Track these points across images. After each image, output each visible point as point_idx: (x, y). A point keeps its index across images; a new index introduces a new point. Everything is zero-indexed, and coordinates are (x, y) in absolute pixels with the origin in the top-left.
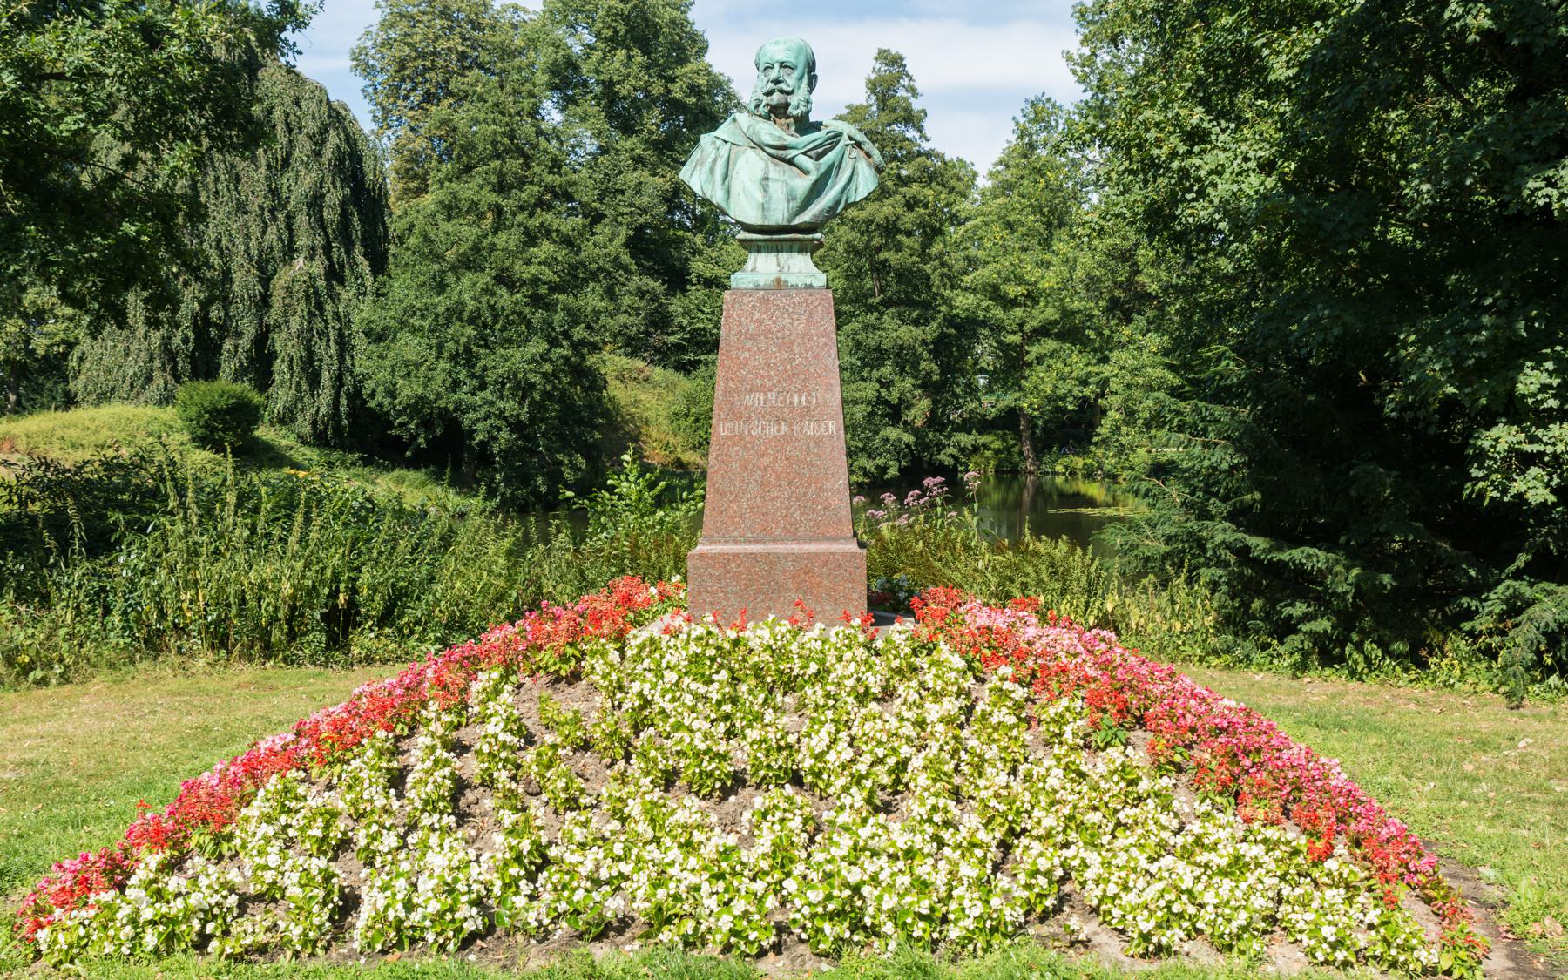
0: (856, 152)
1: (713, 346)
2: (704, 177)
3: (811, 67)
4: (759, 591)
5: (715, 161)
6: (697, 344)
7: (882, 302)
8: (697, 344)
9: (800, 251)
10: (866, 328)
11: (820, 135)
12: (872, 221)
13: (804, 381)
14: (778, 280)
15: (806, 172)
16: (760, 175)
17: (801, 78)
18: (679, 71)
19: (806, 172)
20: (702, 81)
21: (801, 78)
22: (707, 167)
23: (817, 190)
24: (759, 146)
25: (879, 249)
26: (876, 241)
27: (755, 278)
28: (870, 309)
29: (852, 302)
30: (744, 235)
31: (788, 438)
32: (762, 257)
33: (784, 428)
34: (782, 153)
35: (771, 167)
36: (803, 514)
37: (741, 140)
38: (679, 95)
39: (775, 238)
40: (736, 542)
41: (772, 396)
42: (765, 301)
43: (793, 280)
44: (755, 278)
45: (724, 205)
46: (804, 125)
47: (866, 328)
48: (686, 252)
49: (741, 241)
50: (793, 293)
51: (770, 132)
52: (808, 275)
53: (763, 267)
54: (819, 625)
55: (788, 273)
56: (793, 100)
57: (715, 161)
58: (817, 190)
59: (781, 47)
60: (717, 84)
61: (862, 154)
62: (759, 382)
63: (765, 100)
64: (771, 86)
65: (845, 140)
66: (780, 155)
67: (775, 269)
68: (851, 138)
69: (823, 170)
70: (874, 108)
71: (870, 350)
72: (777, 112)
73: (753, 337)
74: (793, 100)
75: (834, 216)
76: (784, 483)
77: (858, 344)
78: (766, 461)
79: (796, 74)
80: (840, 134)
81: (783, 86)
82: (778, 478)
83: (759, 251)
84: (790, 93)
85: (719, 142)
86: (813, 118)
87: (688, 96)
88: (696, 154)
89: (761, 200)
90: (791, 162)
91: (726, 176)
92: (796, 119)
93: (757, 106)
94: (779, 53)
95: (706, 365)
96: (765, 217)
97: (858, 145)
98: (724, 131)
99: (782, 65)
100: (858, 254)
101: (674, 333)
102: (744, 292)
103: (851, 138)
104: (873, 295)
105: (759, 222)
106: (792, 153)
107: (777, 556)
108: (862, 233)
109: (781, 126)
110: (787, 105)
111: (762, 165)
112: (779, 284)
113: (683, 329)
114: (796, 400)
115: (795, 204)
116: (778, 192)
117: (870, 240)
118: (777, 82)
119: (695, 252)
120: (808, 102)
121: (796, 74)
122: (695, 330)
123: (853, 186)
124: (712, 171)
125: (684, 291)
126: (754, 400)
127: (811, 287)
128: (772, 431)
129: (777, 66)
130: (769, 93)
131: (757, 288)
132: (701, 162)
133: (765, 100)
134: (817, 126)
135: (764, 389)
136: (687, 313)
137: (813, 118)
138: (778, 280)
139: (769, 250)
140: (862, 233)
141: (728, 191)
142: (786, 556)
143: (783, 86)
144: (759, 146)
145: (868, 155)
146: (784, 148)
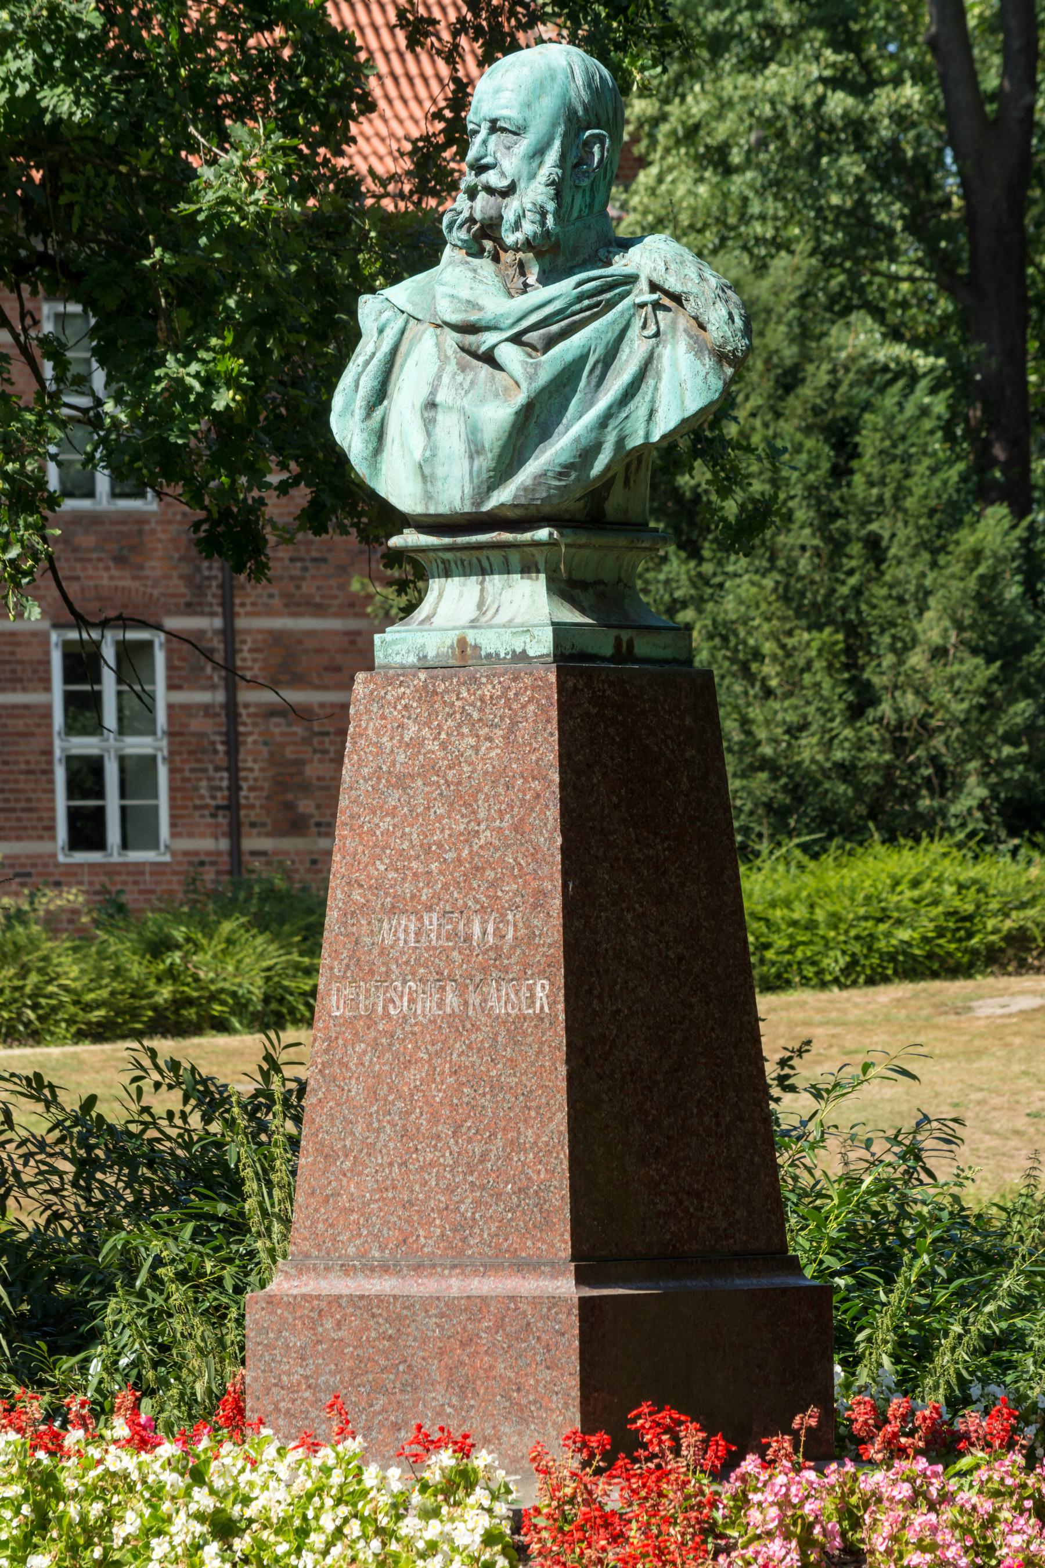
4: (378, 1388)
13: (493, 885)
14: (462, 642)
17: (539, 152)
21: (539, 152)
23: (534, 421)
31: (459, 1023)
33: (451, 999)
34: (470, 339)
36: (478, 1203)
40: (347, 1270)
41: (430, 921)
54: (353, 1445)
62: (408, 888)
69: (544, 377)
73: (401, 782)
76: (445, 1130)
78: (414, 1075)
79: (524, 145)
81: (491, 178)
82: (435, 1119)
83: (447, 574)
96: (428, 497)
106: (489, 339)
107: (408, 1302)
114: (477, 930)
115: (486, 462)
123: (639, 407)
126: (399, 932)
127: (521, 657)
128: (427, 1007)
135: (417, 908)
139: (467, 571)
141: (380, 435)
142: (427, 1303)
143: (491, 178)
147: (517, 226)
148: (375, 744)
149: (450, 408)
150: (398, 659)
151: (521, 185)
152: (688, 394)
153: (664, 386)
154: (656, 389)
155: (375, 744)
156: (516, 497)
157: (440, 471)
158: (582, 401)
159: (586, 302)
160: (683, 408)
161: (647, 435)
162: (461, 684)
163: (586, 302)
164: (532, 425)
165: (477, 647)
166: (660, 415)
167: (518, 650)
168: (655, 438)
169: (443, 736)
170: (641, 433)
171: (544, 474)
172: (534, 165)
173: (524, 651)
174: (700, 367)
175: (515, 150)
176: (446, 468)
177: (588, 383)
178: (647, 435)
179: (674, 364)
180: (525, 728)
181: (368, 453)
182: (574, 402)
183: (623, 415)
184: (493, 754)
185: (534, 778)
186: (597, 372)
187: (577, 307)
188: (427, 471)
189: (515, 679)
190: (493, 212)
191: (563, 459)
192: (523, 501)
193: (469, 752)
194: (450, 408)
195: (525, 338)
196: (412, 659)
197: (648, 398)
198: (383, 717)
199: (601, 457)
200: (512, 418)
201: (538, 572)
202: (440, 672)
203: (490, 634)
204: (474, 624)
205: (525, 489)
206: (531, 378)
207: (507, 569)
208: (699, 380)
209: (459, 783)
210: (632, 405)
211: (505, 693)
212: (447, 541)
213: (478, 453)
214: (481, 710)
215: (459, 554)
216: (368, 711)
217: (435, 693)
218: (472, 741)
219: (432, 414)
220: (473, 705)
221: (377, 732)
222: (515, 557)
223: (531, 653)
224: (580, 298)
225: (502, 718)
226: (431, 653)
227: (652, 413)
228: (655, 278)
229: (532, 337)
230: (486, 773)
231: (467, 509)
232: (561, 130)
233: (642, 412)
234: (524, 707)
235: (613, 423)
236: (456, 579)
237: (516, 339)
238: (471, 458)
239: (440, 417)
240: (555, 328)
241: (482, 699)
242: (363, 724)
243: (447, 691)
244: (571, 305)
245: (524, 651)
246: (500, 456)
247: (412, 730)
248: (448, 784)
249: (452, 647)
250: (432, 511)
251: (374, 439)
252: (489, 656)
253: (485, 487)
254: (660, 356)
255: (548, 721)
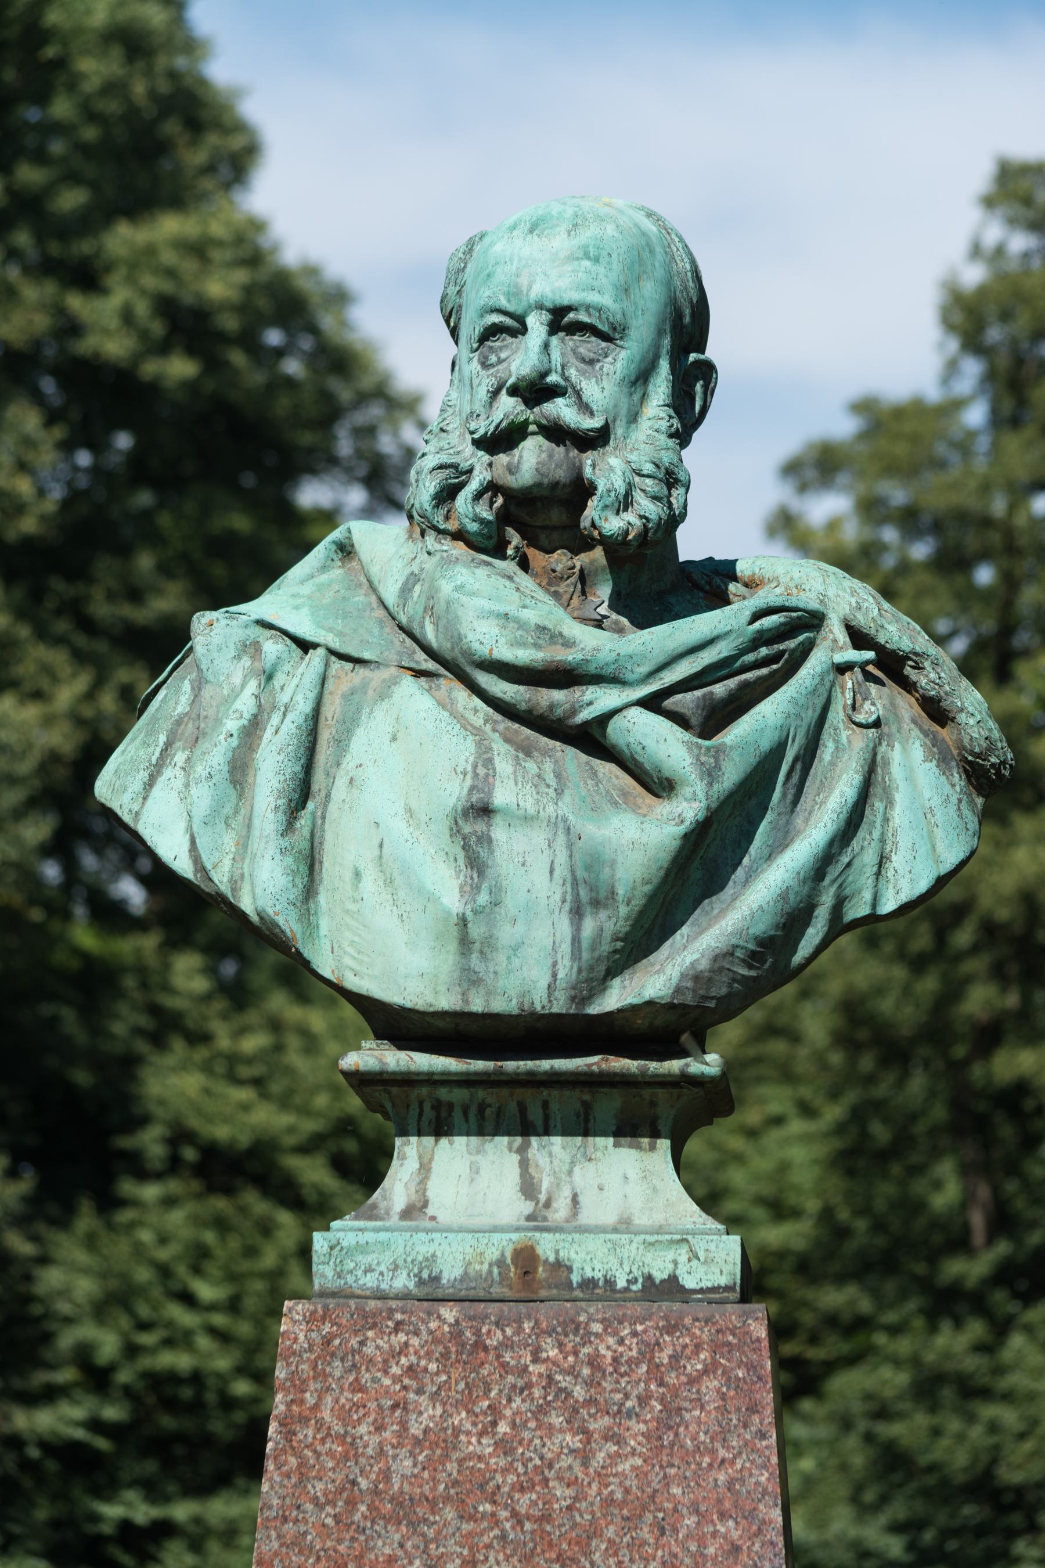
0: (881, 698)
1: (241, 1458)
2: (202, 797)
3: (687, 325)
5: (253, 729)
6: (160, 1446)
7: (1004, 1275)
8: (160, 1446)
9: (629, 1128)
10: (930, 1386)
11: (722, 625)
12: (960, 911)
14: (526, 1259)
15: (658, 785)
16: (454, 792)
17: (642, 377)
18: (123, 238)
19: (658, 785)
20: (219, 287)
21: (642, 377)
22: (217, 755)
23: (704, 862)
24: (452, 665)
25: (990, 1036)
26: (980, 1000)
27: (422, 1246)
28: (947, 1303)
29: (864, 1269)
30: (373, 1056)
32: (453, 1154)
35: (501, 750)
37: (372, 639)
38: (116, 348)
39: (516, 1069)
42: (465, 1350)
43: (589, 1258)
44: (422, 1246)
45: (288, 922)
46: (656, 578)
47: (930, 1386)
48: (124, 1022)
49: (360, 1080)
50: (592, 1315)
51: (497, 607)
52: (662, 1236)
53: (460, 1196)
55: (573, 1226)
56: (607, 471)
57: (253, 729)
58: (704, 862)
59: (560, 242)
60: (289, 302)
61: (907, 706)
63: (482, 469)
64: (508, 407)
65: (832, 647)
66: (543, 707)
67: (512, 1207)
68: (859, 638)
69: (731, 774)
70: (976, 415)
71: (944, 1491)
72: (535, 522)
73: (405, 1511)
74: (607, 471)
75: (784, 974)
77: (893, 1463)
79: (620, 361)
80: (812, 621)
83: (441, 1129)
84: (595, 440)
85: (273, 648)
86: (692, 545)
87: (163, 349)
88: (174, 697)
89: (452, 901)
90: (591, 739)
91: (302, 793)
92: (618, 550)
93: (447, 494)
94: (548, 271)
95: (196, 1546)
96: (470, 979)
97: (892, 666)
98: (291, 600)
99: (561, 320)
100: (895, 1053)
101: (50, 1395)
102: (373, 1310)
103: (859, 638)
104: (960, 1243)
105: (446, 1001)
106: (602, 699)
108: (918, 965)
109: (551, 581)
110: (581, 490)
111: (465, 750)
112: (529, 1279)
113: (97, 1378)
115: (604, 926)
116: (529, 868)
117: (953, 992)
118: (536, 391)
119: (165, 1026)
120: (671, 479)
121: (620, 361)
122: (161, 1382)
123: (864, 850)
124: (240, 770)
125: (109, 1203)
127: (671, 1288)
129: (537, 324)
130: (501, 440)
131: (431, 1293)
132: (190, 733)
133: (482, 469)
134: (712, 583)
136: (116, 1300)
137: (692, 545)
138: (526, 1259)
139: (485, 1123)
140: (918, 965)
143: (562, 410)
144: (452, 665)
145: (936, 712)
146: (565, 677)
147: (625, 503)
148: (341, 1438)
149: (528, 819)
150: (370, 1281)
151: (619, 430)
152: (939, 833)
153: (900, 815)
154: (886, 820)
155: (341, 1438)
156: (678, 990)
157: (506, 934)
158: (774, 827)
159: (764, 651)
160: (938, 861)
161: (874, 904)
162: (539, 1332)
163: (764, 651)
164: (697, 862)
165: (560, 1267)
166: (898, 861)
167: (659, 1276)
168: (888, 906)
169: (503, 1428)
170: (867, 895)
171: (729, 954)
172: (636, 397)
173: (673, 1279)
174: (948, 789)
175: (607, 365)
176: (520, 928)
177: (784, 795)
178: (874, 904)
179: (910, 779)
180: (698, 1423)
181: (295, 893)
182: (763, 827)
183: (845, 859)
184: (625, 1466)
185: (723, 1516)
186: (795, 778)
187: (750, 658)
188: (476, 931)
189: (670, 1329)
190: (561, 474)
191: (762, 927)
192: (689, 999)
193: (566, 1461)
194: (528, 819)
195: (669, 703)
196: (403, 1282)
197: (876, 835)
198: (357, 1387)
199: (811, 931)
200: (676, 844)
201: (655, 1134)
202: (493, 1308)
203: (595, 1244)
204: (536, 1220)
205: (697, 978)
206: (711, 774)
207: (583, 1126)
208: (952, 810)
209: (545, 1518)
210: (855, 844)
211: (649, 1350)
212: (479, 1065)
213: (596, 904)
214: (589, 1383)
215: (481, 1093)
216: (321, 1375)
217: (480, 1345)
218: (573, 1441)
219: (480, 826)
220: (571, 1371)
221: (344, 1415)
222: (609, 1105)
223: (689, 1282)
224: (760, 640)
225: (643, 1400)
226: (450, 1271)
227: (882, 860)
228: (861, 620)
229: (686, 701)
230: (609, 1502)
231: (560, 1006)
232: (667, 342)
233: (869, 858)
234: (693, 1381)
235: (833, 872)
236: (460, 1141)
237: (652, 703)
238: (577, 913)
239: (499, 832)
240: (720, 689)
241: (594, 1362)
242: (310, 1399)
243: (507, 1344)
244: (743, 652)
245: (673, 1279)
246: (642, 913)
247: (427, 1415)
248: (518, 1519)
249: (500, 1263)
250: (477, 1005)
251: (304, 869)
252: (589, 1284)
253: (602, 968)
254: (886, 763)
255: (753, 1409)
